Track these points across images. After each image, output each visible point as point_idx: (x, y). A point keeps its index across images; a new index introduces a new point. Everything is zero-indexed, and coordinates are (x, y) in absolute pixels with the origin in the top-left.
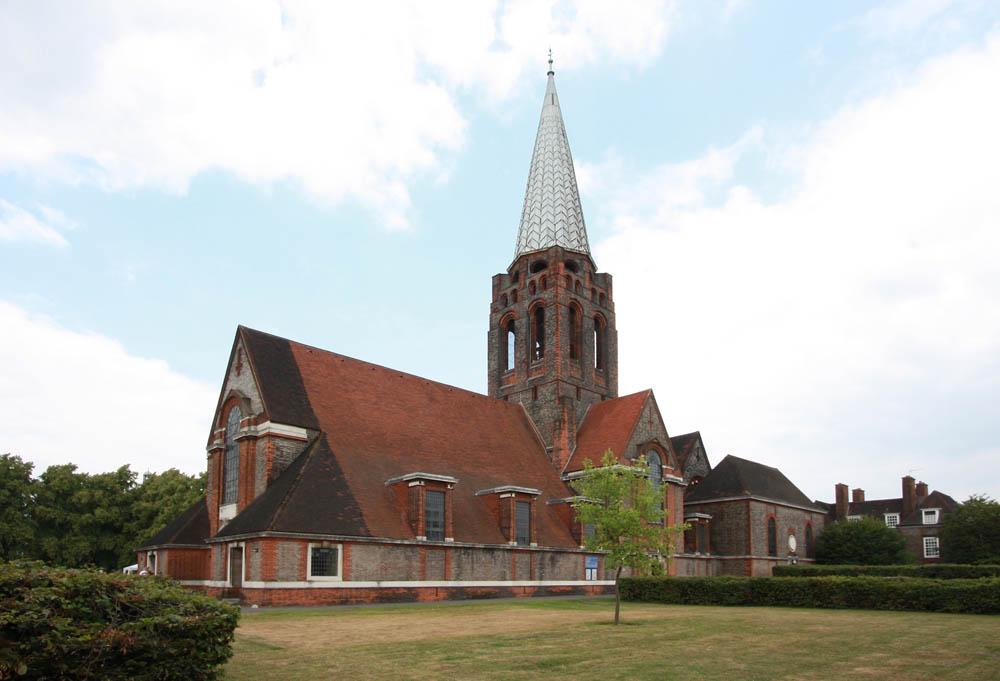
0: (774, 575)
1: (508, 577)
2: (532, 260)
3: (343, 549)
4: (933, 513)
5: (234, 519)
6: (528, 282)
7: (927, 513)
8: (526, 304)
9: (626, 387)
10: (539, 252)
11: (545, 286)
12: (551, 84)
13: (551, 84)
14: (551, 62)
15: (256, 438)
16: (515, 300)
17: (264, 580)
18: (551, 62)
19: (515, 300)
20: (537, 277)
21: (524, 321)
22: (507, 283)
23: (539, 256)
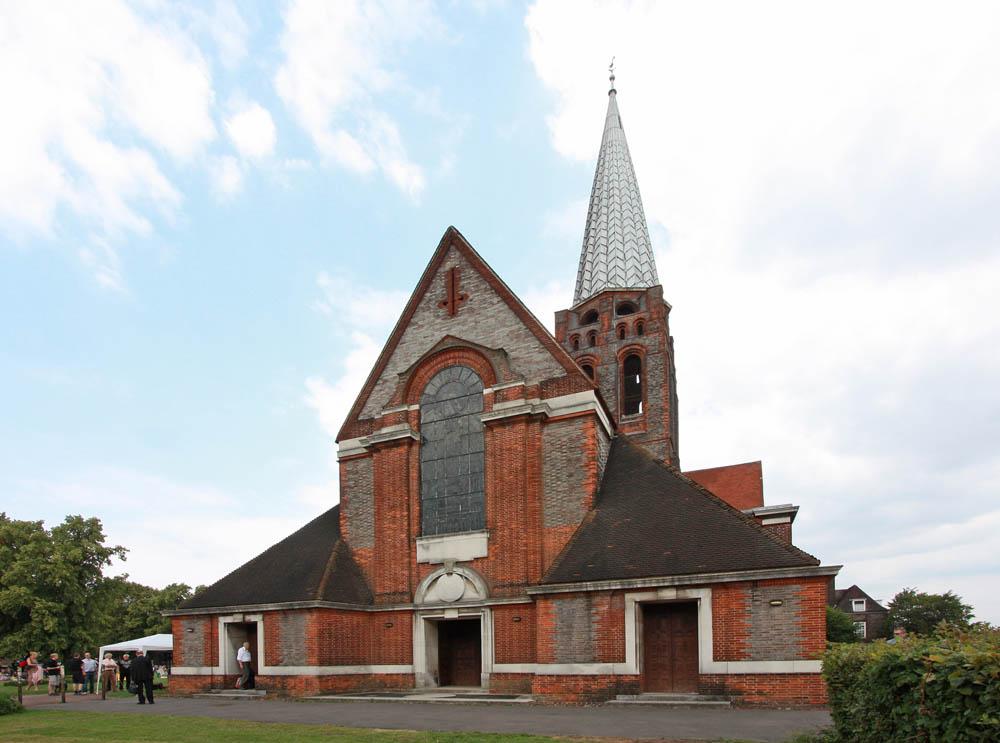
0: (715, 659)
1: (317, 681)
2: (618, 299)
3: (713, 599)
4: (862, 602)
5: (210, 587)
6: (615, 323)
7: (856, 603)
8: (615, 348)
9: (694, 455)
10: (629, 291)
11: (640, 330)
12: (613, 105)
13: (613, 105)
14: (612, 78)
15: (544, 420)
16: (592, 343)
17: (321, 663)
18: (612, 78)
19: (592, 343)
20: (584, 331)
21: (612, 367)
22: (574, 323)
23: (627, 296)
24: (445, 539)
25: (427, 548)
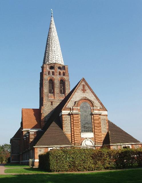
6: (58, 71)
24: (86, 133)
25: (83, 135)
